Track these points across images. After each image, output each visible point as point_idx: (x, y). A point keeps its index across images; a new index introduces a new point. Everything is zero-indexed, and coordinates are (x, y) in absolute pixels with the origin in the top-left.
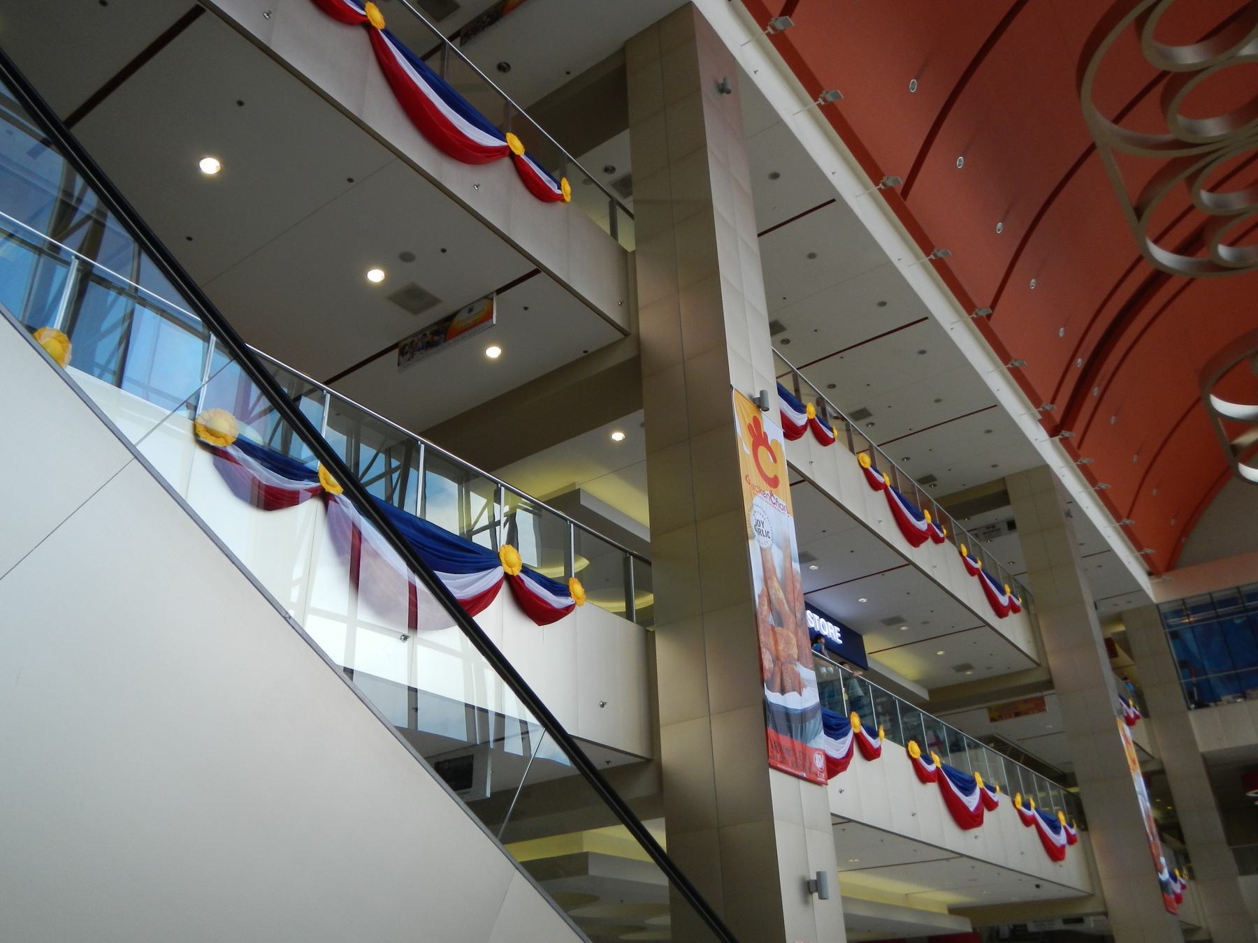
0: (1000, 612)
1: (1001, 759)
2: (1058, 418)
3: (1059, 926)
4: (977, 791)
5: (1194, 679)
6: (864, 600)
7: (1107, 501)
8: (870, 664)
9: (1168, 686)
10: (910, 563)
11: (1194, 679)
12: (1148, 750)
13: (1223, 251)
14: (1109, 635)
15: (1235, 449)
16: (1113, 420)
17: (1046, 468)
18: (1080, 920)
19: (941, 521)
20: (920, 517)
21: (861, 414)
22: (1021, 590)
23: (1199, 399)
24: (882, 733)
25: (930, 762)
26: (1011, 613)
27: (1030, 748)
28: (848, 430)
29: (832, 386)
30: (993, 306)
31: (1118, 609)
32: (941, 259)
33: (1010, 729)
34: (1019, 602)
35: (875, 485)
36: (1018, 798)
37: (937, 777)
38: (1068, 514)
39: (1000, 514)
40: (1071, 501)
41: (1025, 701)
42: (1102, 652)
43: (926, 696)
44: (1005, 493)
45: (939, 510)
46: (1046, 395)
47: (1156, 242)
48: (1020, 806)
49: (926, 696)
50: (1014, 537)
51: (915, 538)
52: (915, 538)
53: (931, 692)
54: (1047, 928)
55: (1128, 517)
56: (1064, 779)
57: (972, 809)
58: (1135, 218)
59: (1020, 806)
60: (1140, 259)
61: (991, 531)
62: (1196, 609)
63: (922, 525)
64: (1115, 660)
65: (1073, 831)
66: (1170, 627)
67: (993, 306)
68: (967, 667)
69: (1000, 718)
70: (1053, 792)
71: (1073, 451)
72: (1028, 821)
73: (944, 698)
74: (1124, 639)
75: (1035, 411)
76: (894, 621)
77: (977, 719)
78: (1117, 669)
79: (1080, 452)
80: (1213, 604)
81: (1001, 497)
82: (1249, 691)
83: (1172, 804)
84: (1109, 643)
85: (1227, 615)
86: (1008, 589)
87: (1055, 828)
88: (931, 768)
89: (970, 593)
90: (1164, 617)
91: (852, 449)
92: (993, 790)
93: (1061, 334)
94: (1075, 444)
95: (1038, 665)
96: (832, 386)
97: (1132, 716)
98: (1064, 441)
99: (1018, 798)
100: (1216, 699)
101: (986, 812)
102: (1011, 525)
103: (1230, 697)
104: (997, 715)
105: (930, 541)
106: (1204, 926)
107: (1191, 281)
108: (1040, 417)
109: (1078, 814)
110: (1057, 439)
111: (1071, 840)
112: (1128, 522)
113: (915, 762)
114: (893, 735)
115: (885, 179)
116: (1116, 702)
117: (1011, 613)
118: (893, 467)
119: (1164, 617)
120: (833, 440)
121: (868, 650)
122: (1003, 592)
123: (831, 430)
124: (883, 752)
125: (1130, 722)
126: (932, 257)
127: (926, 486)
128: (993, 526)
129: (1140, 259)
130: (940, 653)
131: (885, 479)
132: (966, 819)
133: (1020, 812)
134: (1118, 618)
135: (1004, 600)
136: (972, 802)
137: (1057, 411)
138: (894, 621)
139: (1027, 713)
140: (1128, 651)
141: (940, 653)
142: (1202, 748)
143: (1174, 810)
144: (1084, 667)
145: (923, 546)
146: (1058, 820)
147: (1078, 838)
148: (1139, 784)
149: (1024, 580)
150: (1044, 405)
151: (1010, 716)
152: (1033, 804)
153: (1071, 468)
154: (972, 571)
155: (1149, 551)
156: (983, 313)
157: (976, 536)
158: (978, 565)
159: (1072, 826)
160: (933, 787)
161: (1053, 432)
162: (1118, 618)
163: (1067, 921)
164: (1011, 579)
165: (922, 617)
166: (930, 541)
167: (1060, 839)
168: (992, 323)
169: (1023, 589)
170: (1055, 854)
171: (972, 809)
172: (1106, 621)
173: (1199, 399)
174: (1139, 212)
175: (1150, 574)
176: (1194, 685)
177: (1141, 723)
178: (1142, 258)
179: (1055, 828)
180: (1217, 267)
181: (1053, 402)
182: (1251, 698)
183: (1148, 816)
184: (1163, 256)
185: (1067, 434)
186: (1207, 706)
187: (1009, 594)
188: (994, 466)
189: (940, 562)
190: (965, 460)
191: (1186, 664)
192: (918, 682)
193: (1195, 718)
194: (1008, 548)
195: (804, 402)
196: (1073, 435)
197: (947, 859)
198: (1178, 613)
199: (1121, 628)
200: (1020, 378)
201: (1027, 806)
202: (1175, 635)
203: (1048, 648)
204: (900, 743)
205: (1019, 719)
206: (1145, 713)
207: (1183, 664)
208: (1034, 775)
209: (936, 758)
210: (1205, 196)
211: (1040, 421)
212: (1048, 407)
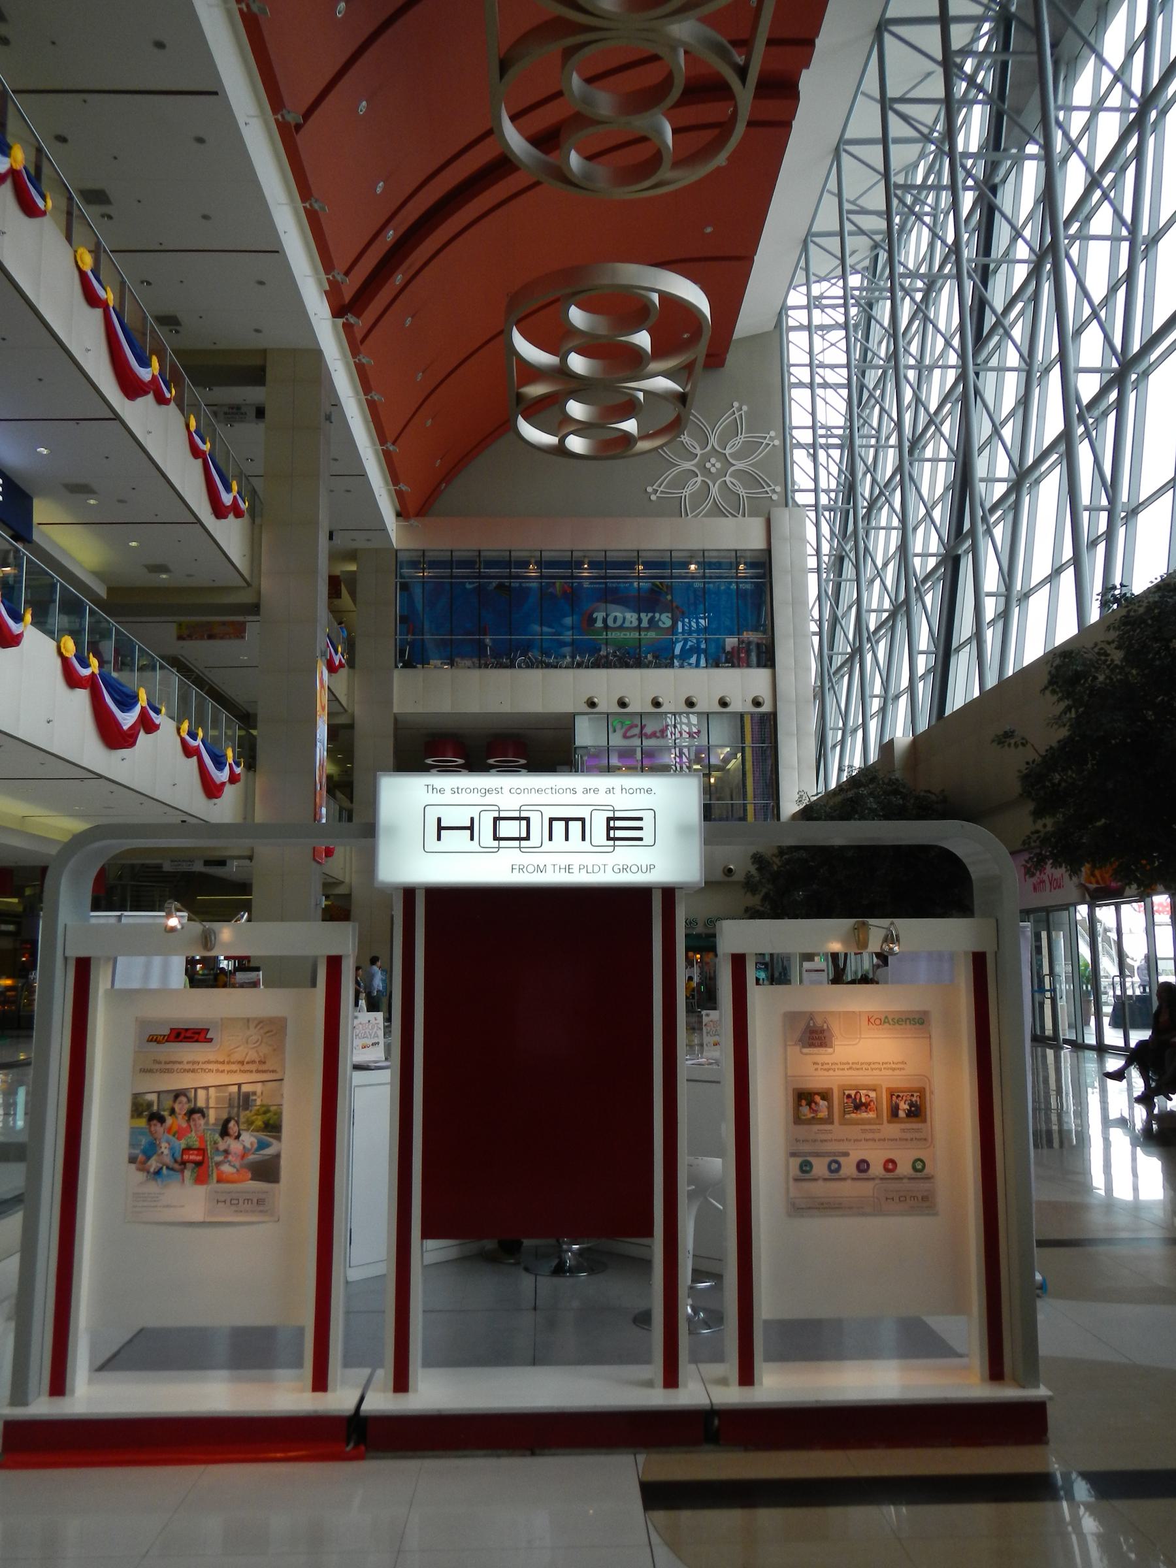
0: (219, 511)
1: (175, 678)
2: (347, 297)
3: (199, 867)
4: (138, 709)
5: (410, 637)
6: (45, 452)
7: (375, 413)
8: (36, 537)
9: (381, 639)
10: (117, 417)
11: (410, 637)
12: (344, 703)
13: (575, 160)
14: (337, 572)
15: (520, 397)
16: (409, 321)
17: (317, 354)
18: (222, 863)
19: (173, 378)
20: (145, 363)
21: (96, 197)
22: (253, 495)
23: (501, 332)
24: (28, 617)
25: (85, 664)
26: (231, 516)
27: (216, 678)
28: (69, 214)
29: (62, 139)
30: (307, 115)
31: (355, 545)
32: (337, 281)
33: (199, 652)
34: (244, 506)
35: (92, 299)
36: (185, 726)
37: (90, 683)
38: (328, 418)
39: (250, 395)
40: (337, 404)
41: (224, 623)
42: (323, 589)
43: (102, 592)
44: (263, 369)
45: (173, 366)
46: (341, 264)
47: (513, 118)
48: (184, 734)
49: (102, 592)
50: (261, 426)
51: (131, 387)
52: (131, 387)
53: (110, 590)
54: (184, 868)
55: (394, 443)
56: (246, 719)
57: (125, 728)
58: (497, 76)
59: (184, 734)
60: (490, 132)
61: (233, 413)
62: (433, 564)
63: (145, 374)
64: (336, 602)
65: (238, 770)
66: (402, 577)
67: (307, 115)
68: (163, 569)
69: (190, 637)
70: (228, 731)
71: (354, 343)
72: (188, 751)
73: (128, 601)
74: (352, 578)
75: (324, 277)
76: (81, 489)
77: (163, 633)
78: (334, 611)
79: (362, 348)
80: (450, 564)
81: (255, 375)
82: (458, 660)
83: (352, 763)
84: (335, 584)
85: (463, 577)
86: (235, 487)
87: (219, 763)
88: (85, 672)
89: (188, 479)
90: (399, 565)
91: (69, 238)
92: (158, 711)
93: (379, 190)
94: (359, 336)
95: (249, 585)
96: (62, 139)
97: (337, 663)
98: (347, 327)
99: (185, 726)
100: (424, 662)
101: (142, 734)
102: (260, 413)
103: (438, 662)
104: (187, 633)
105: (150, 397)
106: (347, 880)
107: (537, 184)
108: (327, 288)
109: (249, 755)
110: (340, 321)
111: (233, 779)
112: (391, 448)
113: (65, 661)
114: (40, 622)
115: (284, 111)
116: (322, 641)
117: (231, 516)
118: (123, 283)
119: (399, 565)
120: (44, 213)
121: (37, 518)
122: (228, 489)
123: (44, 198)
124: (25, 641)
125: (332, 668)
126: (307, 205)
127: (167, 328)
128: (238, 408)
129: (490, 132)
130: (134, 544)
131: (108, 295)
132: (114, 737)
133: (183, 741)
134: (352, 555)
135: (227, 499)
136: (127, 720)
137: (350, 286)
138: (81, 489)
139: (222, 638)
140: (353, 594)
141: (134, 544)
142: (395, 710)
143: (352, 768)
144: (297, 600)
145: (140, 400)
146: (225, 756)
147: (242, 777)
148: (322, 732)
149: (258, 483)
150: (335, 273)
151: (202, 638)
152: (201, 734)
153: (347, 364)
154: (196, 452)
155: (404, 488)
156: (292, 118)
157: (215, 414)
158: (206, 447)
159: (238, 765)
160: (82, 696)
161: (338, 311)
162: (352, 555)
163: (207, 863)
164: (241, 476)
165: (118, 491)
166: (150, 397)
167: (222, 776)
168: (300, 139)
169: (254, 493)
170: (212, 790)
171: (125, 728)
172: (336, 556)
173: (501, 332)
174: (504, 66)
175: (398, 515)
176: (408, 643)
177: (344, 672)
178: (492, 132)
179: (219, 763)
180: (562, 176)
181: (347, 273)
182: (458, 667)
183: (321, 765)
184: (514, 139)
185: (352, 319)
186: (415, 667)
187: (235, 493)
188: (257, 331)
189: (159, 430)
190: (224, 316)
191: (407, 620)
192: (97, 574)
193: (400, 678)
194: (248, 441)
195: (10, 140)
196: (360, 324)
197: (82, 779)
198: (414, 564)
199: (353, 567)
200: (315, 224)
201: (194, 736)
202: (405, 587)
203: (264, 568)
204: (50, 633)
205: (211, 642)
206: (351, 663)
207: (404, 619)
208: (210, 703)
209: (94, 662)
210: (576, 81)
211: (326, 292)
212: (339, 278)
